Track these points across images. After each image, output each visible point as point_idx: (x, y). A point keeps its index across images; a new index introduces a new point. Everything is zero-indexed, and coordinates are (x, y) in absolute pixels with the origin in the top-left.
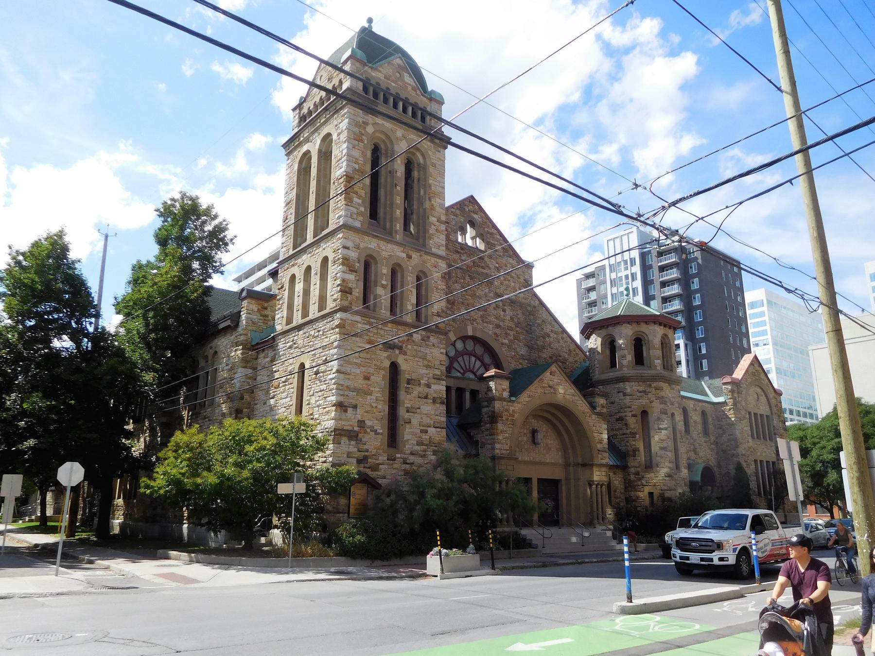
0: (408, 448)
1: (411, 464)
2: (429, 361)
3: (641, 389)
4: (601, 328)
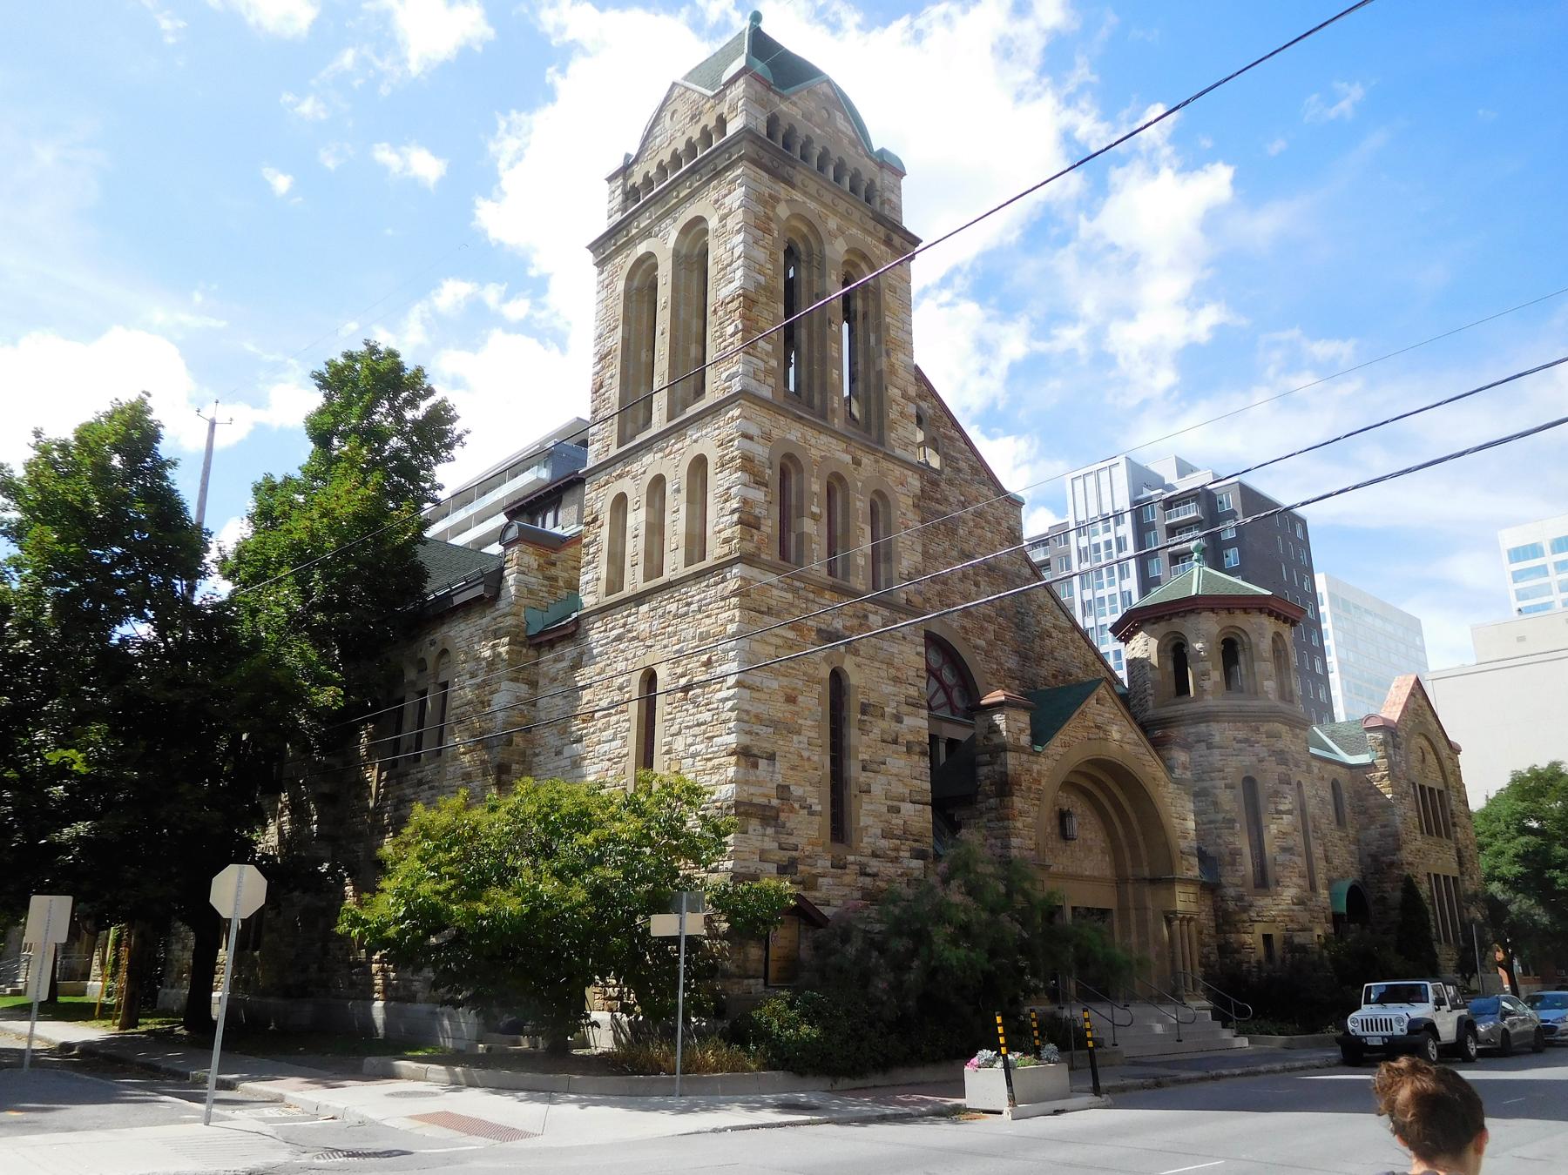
0: (867, 843)
1: (874, 875)
2: (898, 669)
3: (1240, 735)
4: (1158, 619)
